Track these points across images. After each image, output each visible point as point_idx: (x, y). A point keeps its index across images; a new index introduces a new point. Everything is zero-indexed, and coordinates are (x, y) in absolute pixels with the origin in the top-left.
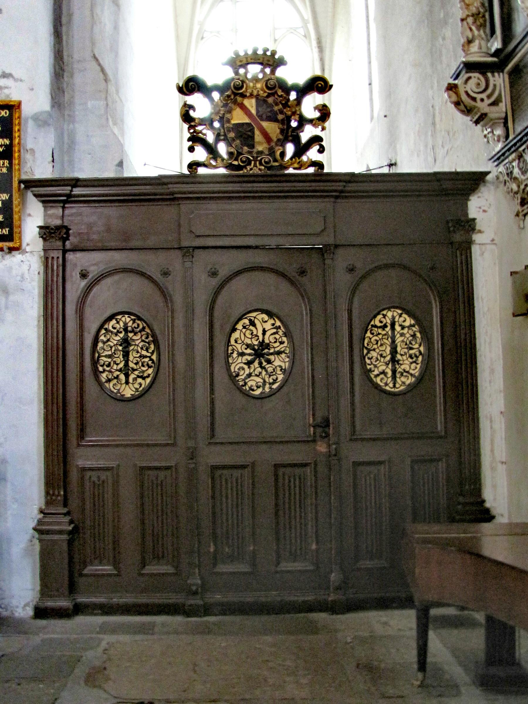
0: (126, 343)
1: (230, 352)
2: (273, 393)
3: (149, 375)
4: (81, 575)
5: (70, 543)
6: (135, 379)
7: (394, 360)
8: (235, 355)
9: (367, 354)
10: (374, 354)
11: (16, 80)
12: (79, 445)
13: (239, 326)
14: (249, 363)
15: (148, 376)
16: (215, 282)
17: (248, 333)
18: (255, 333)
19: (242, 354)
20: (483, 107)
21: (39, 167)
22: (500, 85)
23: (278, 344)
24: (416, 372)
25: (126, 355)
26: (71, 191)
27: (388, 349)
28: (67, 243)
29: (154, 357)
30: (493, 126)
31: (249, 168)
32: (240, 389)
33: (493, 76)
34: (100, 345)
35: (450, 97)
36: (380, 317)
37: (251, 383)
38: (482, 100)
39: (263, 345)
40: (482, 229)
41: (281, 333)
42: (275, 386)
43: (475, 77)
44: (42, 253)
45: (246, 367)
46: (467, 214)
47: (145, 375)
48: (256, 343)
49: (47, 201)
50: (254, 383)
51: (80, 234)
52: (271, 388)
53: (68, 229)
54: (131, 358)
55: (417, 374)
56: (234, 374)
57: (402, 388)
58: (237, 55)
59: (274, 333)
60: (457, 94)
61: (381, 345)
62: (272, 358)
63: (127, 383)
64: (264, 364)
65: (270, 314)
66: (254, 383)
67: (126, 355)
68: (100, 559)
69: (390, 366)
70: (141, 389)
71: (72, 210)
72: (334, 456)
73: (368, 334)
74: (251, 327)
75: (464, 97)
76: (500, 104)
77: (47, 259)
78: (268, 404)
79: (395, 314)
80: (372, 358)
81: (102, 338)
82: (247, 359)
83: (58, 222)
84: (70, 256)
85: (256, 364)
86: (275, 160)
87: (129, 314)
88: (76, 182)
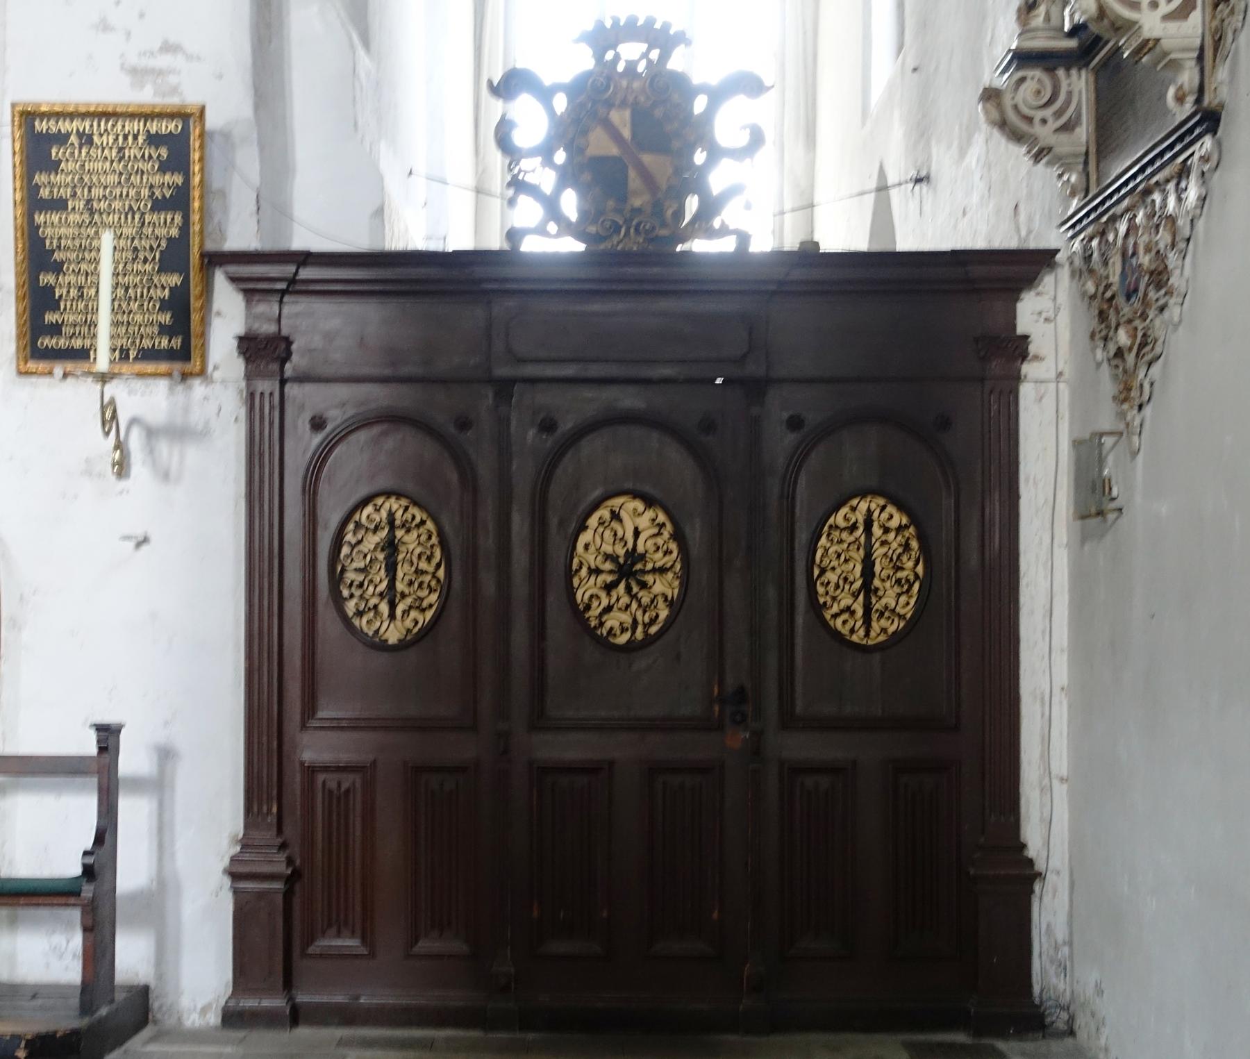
0: (391, 546)
1: (575, 566)
2: (649, 640)
3: (431, 606)
4: (304, 954)
5: (288, 895)
6: (406, 613)
7: (868, 589)
8: (584, 572)
9: (819, 576)
10: (832, 577)
11: (189, 58)
12: (304, 726)
13: (593, 521)
14: (609, 588)
15: (431, 606)
16: (549, 442)
17: (608, 534)
18: (620, 534)
19: (596, 571)
20: (1045, 134)
21: (241, 233)
22: (1080, 92)
23: (660, 554)
24: (908, 612)
25: (391, 569)
26: (296, 273)
27: (859, 568)
28: (288, 366)
29: (441, 573)
30: (1067, 168)
31: (615, 239)
32: (591, 632)
33: (1069, 76)
34: (345, 550)
35: (986, 112)
36: (844, 510)
37: (612, 621)
38: (1044, 121)
39: (634, 556)
40: (1042, 353)
41: (666, 535)
42: (653, 630)
43: (1033, 78)
44: (243, 384)
45: (603, 595)
46: (1014, 327)
47: (425, 604)
48: (621, 552)
49: (251, 291)
50: (616, 624)
51: (310, 351)
52: (646, 633)
53: (288, 342)
54: (400, 574)
55: (908, 616)
56: (581, 607)
57: (882, 638)
58: (600, 25)
59: (654, 535)
60: (999, 106)
61: (846, 561)
62: (649, 579)
63: (392, 616)
64: (635, 589)
65: (650, 502)
66: (616, 624)
67: (391, 569)
68: (340, 925)
69: (861, 597)
70: (416, 630)
71: (295, 307)
72: (756, 750)
73: (823, 540)
74: (615, 525)
75: (1012, 116)
76: (1078, 130)
77: (251, 395)
78: (641, 662)
79: (873, 506)
80: (828, 583)
81: (349, 537)
82: (605, 581)
83: (270, 328)
84: (292, 390)
85: (622, 587)
86: (664, 225)
87: (399, 495)
88: (305, 258)
